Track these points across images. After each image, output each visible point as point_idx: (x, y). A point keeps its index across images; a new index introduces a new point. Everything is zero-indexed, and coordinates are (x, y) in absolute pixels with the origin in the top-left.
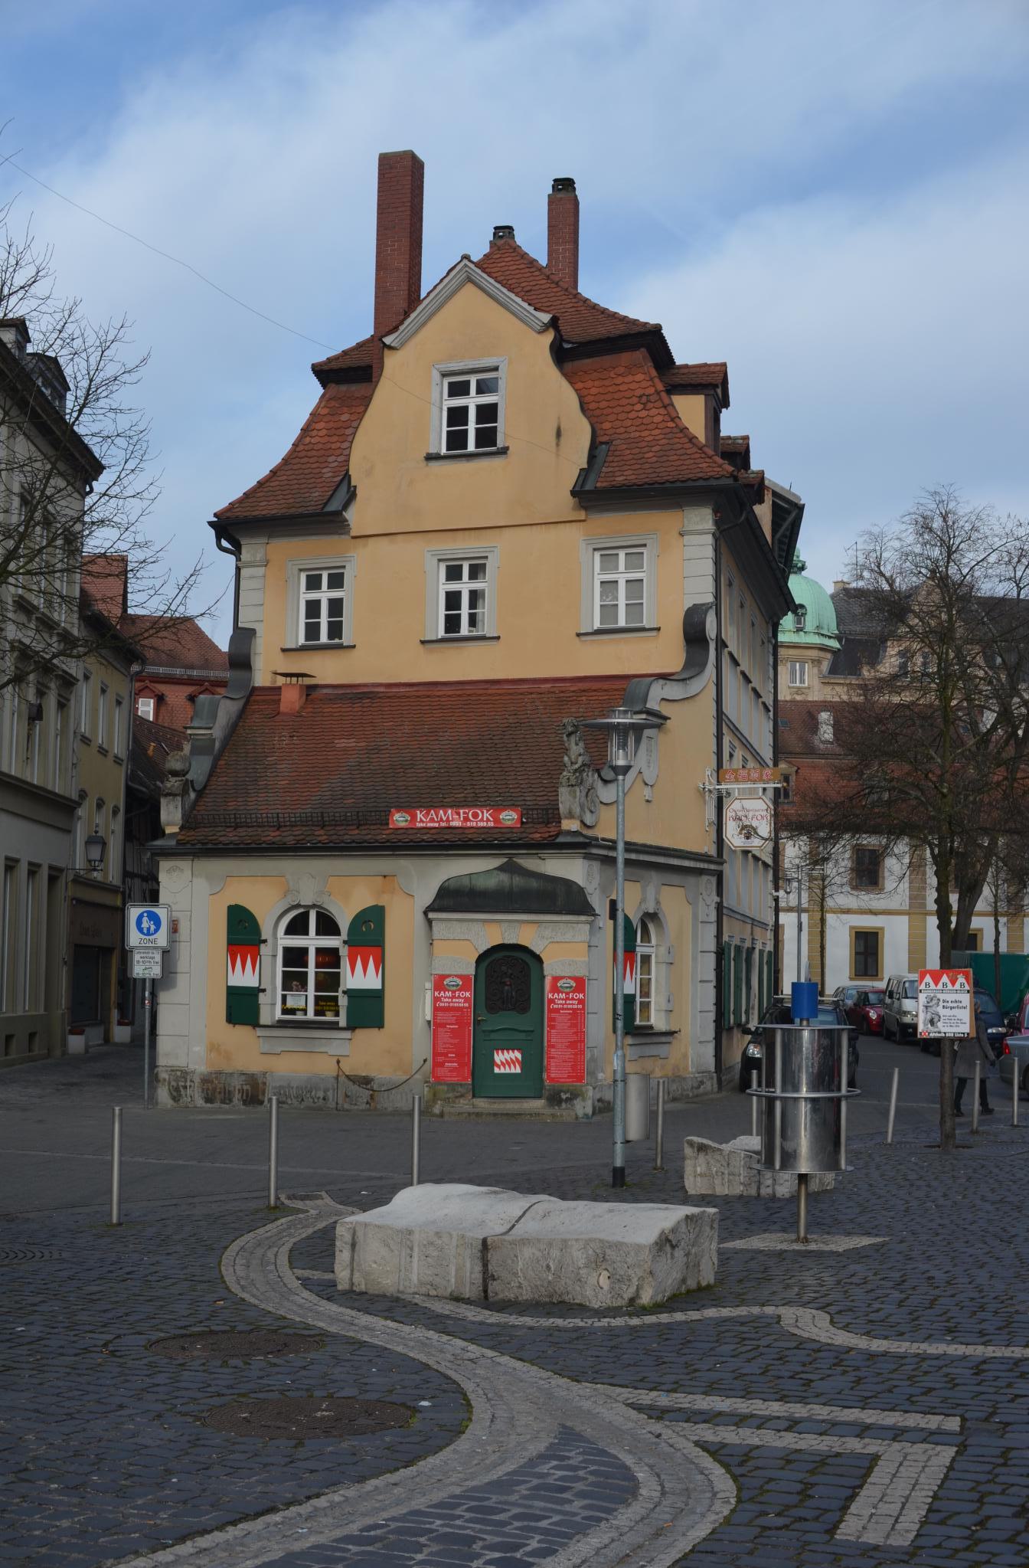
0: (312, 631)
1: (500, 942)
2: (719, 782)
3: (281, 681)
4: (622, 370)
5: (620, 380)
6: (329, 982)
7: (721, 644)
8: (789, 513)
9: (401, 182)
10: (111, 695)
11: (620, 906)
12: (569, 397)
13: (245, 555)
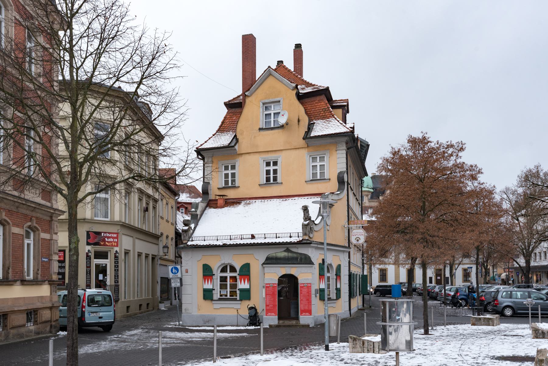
0: (226, 182)
1: (296, 275)
2: (348, 224)
3: (218, 197)
4: (317, 101)
5: (316, 104)
6: (234, 286)
7: (348, 184)
8: (365, 147)
9: (249, 44)
10: (170, 206)
11: (325, 261)
12: (301, 109)
13: (206, 160)
